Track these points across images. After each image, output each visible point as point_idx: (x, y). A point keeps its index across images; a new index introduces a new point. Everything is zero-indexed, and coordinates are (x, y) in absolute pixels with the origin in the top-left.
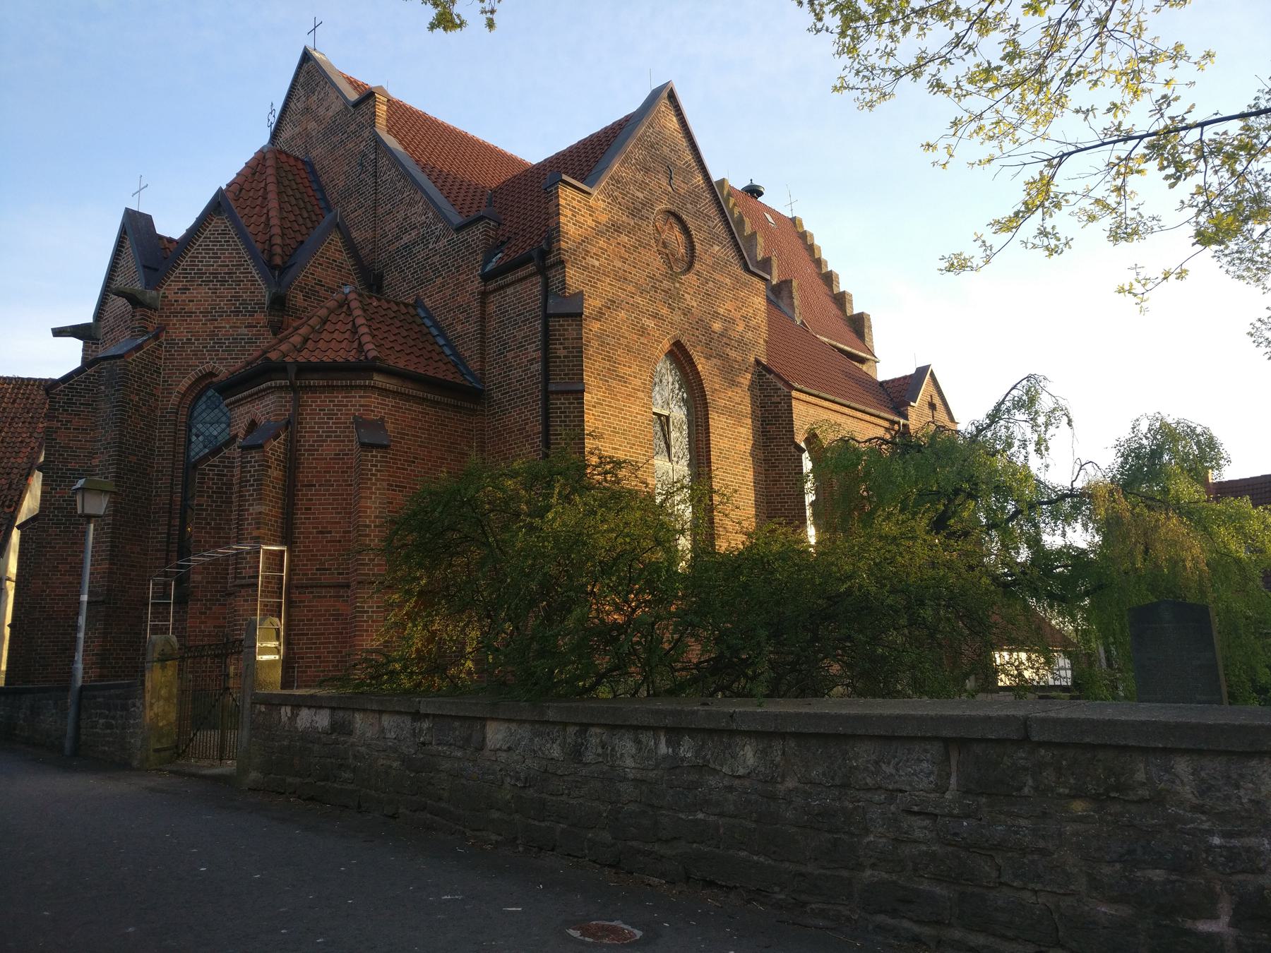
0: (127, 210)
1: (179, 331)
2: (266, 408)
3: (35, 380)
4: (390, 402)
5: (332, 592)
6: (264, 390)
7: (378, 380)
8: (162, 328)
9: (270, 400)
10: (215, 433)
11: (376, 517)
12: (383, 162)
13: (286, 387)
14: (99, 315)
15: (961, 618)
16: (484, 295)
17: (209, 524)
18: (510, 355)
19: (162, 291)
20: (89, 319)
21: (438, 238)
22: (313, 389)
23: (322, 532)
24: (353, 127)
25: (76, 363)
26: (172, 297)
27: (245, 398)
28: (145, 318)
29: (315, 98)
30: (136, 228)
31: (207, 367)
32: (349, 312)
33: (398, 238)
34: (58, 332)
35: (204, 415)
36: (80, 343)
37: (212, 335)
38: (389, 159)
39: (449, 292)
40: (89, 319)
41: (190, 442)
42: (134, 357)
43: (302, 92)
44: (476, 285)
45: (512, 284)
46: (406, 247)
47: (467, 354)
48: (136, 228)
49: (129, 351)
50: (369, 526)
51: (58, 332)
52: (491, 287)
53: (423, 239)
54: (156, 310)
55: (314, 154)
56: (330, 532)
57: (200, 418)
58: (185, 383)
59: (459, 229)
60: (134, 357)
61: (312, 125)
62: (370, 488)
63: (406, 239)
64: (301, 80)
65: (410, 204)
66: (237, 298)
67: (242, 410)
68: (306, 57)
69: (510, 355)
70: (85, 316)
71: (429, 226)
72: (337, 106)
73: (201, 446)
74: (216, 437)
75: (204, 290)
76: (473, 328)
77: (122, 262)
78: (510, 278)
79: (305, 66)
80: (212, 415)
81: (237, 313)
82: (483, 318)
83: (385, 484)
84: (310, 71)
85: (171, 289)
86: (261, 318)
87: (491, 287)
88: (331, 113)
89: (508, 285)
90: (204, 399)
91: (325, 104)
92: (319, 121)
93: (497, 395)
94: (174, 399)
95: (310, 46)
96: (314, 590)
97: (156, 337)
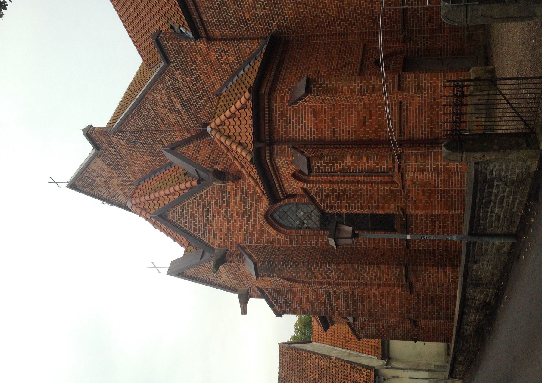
0: (168, 274)
1: (240, 237)
2: (286, 164)
3: (280, 360)
4: (279, 86)
5: (404, 114)
6: (273, 166)
7: (265, 90)
8: (239, 246)
9: (280, 161)
10: (302, 213)
11: (355, 83)
12: (132, 126)
13: (270, 150)
14: (233, 290)
15: (388, 301)
16: (209, 39)
17: (358, 201)
18: (247, 16)
19: (215, 247)
20: (236, 296)
21: (176, 79)
22: (271, 133)
23: (364, 122)
24: (112, 150)
25: (263, 301)
26: (218, 242)
27: (278, 182)
28: (232, 255)
29: (97, 179)
30: (179, 270)
31: (261, 218)
32: (223, 123)
33: (178, 112)
34: (244, 311)
35: (291, 220)
36: (251, 300)
37: (242, 216)
38: (129, 121)
39: (210, 69)
40: (236, 296)
41: (308, 228)
42: (255, 258)
43: (96, 190)
44: (202, 45)
45: (199, 14)
46: (184, 106)
47: (248, 51)
48: (179, 270)
49: (252, 260)
50: (361, 87)
51: (244, 311)
52: (203, 33)
53: (178, 91)
54: (227, 250)
55: (133, 179)
56: (364, 117)
57: (293, 223)
58: (272, 231)
59: (167, 61)
60: (255, 258)
61: (114, 180)
62: (336, 87)
63: (179, 106)
64: (88, 190)
65: (156, 104)
66: (218, 203)
67: (286, 185)
68: (73, 185)
69: (247, 16)
70: (235, 297)
71: (168, 88)
72: (99, 162)
73: (310, 221)
74: (304, 213)
75: (213, 223)
76: (231, 47)
77: (200, 276)
78: (196, 16)
79: (80, 187)
80: (291, 215)
81: (227, 202)
82: (224, 39)
83: (333, 79)
84: (82, 183)
85: (214, 242)
86: (230, 187)
87: (203, 33)
88: (105, 168)
89: (201, 19)
90: (281, 221)
91: (100, 172)
92: (111, 177)
93: (274, 27)
94: (281, 237)
95: (66, 184)
96: (402, 125)
97: (243, 248)
